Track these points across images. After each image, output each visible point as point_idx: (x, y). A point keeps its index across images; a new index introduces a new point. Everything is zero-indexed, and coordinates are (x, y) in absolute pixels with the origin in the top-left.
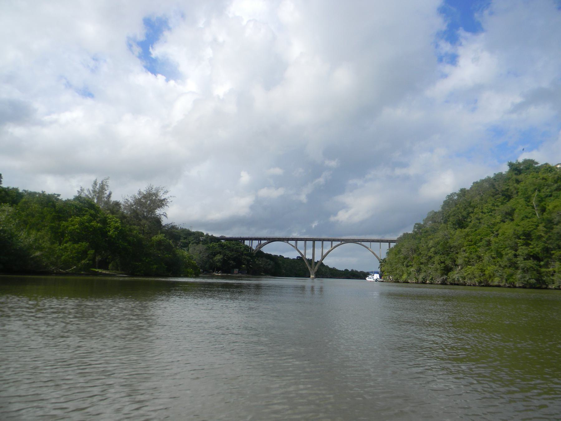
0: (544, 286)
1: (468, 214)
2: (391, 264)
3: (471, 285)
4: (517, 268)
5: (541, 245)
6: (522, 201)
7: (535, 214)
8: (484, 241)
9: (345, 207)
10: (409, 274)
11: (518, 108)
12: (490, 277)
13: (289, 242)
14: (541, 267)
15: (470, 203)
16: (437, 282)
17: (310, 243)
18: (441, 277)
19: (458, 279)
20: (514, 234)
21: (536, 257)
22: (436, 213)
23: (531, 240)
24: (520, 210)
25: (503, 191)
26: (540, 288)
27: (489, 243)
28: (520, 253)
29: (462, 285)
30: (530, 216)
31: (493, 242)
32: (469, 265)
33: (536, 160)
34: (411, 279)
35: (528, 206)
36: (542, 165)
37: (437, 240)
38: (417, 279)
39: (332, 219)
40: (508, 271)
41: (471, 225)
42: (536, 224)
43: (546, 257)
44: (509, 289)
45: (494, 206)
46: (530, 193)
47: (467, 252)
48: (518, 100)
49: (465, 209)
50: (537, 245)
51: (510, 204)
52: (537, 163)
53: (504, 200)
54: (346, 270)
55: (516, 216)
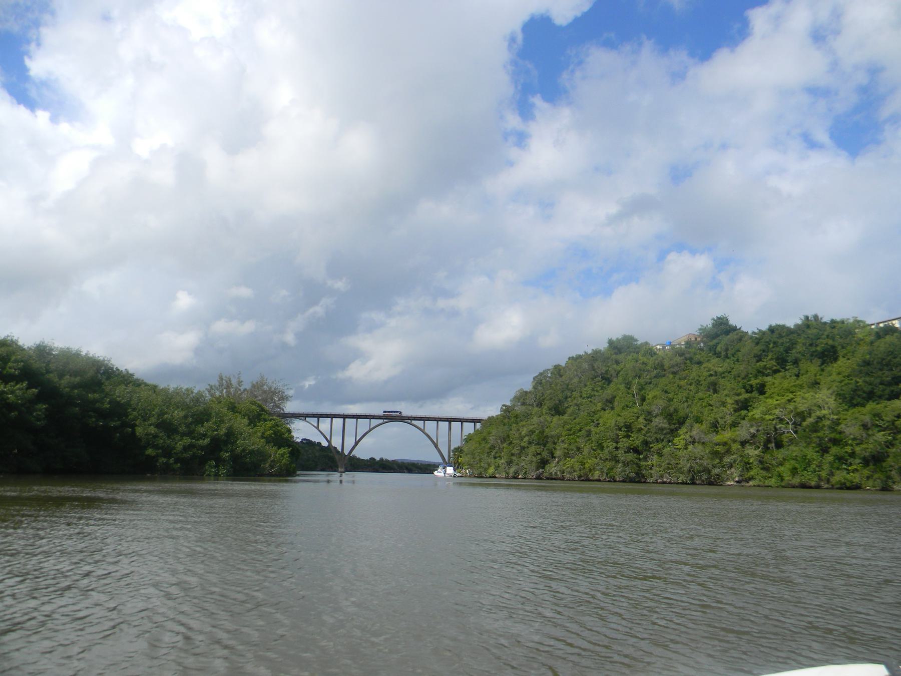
0: (643, 480)
1: (566, 398)
2: (473, 454)
3: (570, 480)
4: (617, 461)
5: (641, 438)
6: (622, 387)
7: (636, 403)
8: (583, 431)
9: (358, 355)
10: (497, 468)
11: (613, 220)
12: (590, 470)
13: (308, 419)
14: (640, 459)
15: (568, 386)
16: (531, 477)
17: (338, 422)
18: (536, 471)
19: (555, 473)
20: (616, 425)
21: (636, 451)
22: (526, 392)
23: (632, 433)
24: (621, 398)
25: (602, 373)
26: (639, 482)
27: (589, 434)
28: (621, 446)
29: (560, 479)
30: (630, 404)
31: (594, 432)
32: (569, 457)
33: (636, 337)
34: (499, 473)
35: (628, 393)
36: (642, 343)
37: (531, 427)
38: (507, 473)
39: (341, 375)
40: (609, 464)
41: (570, 411)
42: (637, 415)
43: (645, 450)
44: (609, 483)
45: (594, 390)
46: (630, 379)
47: (565, 443)
48: (613, 209)
49: (563, 392)
50: (637, 438)
51: (609, 391)
52: (636, 340)
53: (604, 384)
54: (372, 459)
55: (616, 403)
